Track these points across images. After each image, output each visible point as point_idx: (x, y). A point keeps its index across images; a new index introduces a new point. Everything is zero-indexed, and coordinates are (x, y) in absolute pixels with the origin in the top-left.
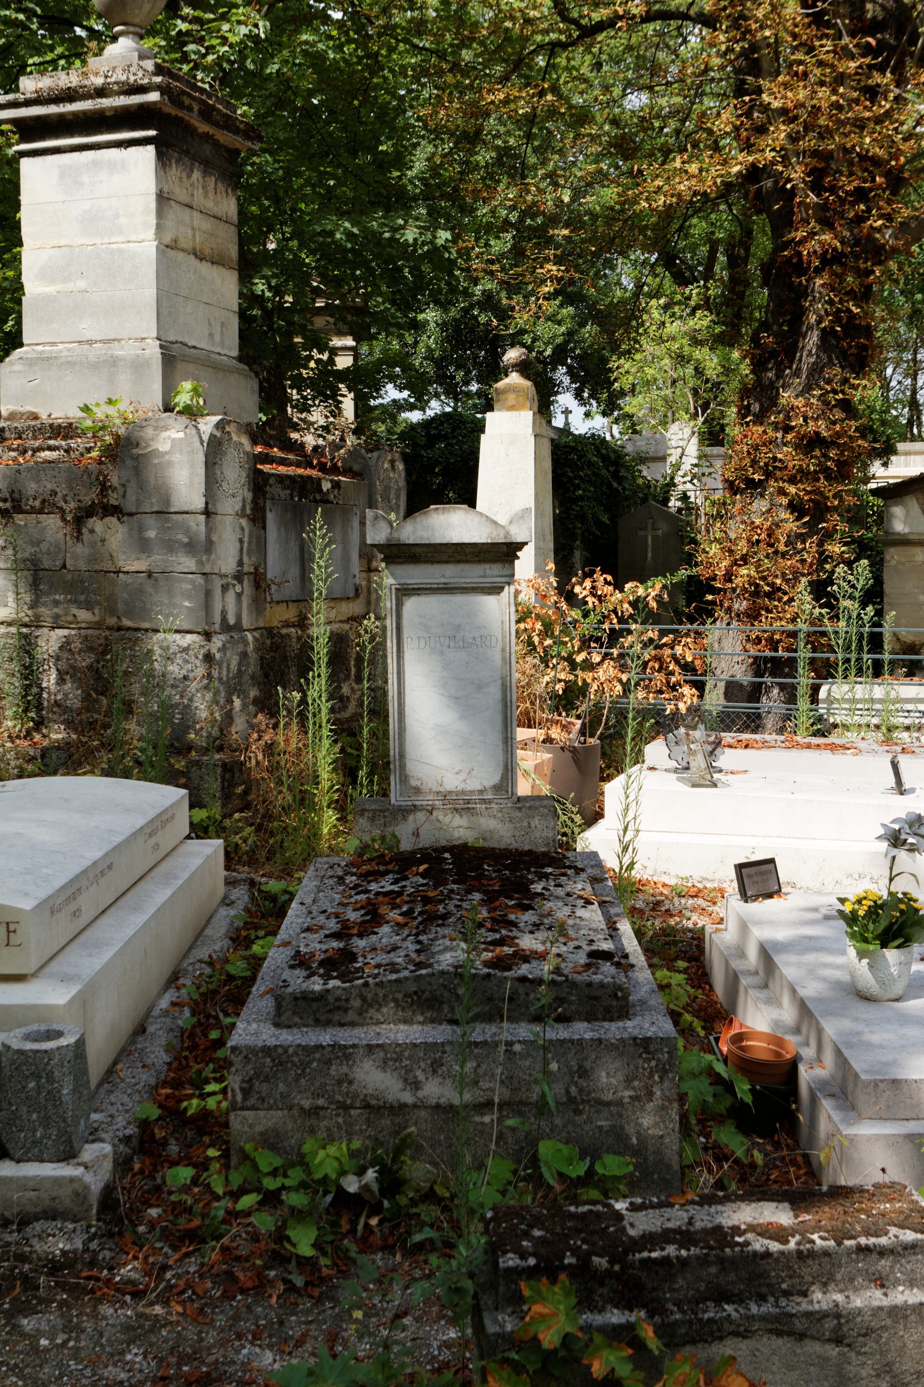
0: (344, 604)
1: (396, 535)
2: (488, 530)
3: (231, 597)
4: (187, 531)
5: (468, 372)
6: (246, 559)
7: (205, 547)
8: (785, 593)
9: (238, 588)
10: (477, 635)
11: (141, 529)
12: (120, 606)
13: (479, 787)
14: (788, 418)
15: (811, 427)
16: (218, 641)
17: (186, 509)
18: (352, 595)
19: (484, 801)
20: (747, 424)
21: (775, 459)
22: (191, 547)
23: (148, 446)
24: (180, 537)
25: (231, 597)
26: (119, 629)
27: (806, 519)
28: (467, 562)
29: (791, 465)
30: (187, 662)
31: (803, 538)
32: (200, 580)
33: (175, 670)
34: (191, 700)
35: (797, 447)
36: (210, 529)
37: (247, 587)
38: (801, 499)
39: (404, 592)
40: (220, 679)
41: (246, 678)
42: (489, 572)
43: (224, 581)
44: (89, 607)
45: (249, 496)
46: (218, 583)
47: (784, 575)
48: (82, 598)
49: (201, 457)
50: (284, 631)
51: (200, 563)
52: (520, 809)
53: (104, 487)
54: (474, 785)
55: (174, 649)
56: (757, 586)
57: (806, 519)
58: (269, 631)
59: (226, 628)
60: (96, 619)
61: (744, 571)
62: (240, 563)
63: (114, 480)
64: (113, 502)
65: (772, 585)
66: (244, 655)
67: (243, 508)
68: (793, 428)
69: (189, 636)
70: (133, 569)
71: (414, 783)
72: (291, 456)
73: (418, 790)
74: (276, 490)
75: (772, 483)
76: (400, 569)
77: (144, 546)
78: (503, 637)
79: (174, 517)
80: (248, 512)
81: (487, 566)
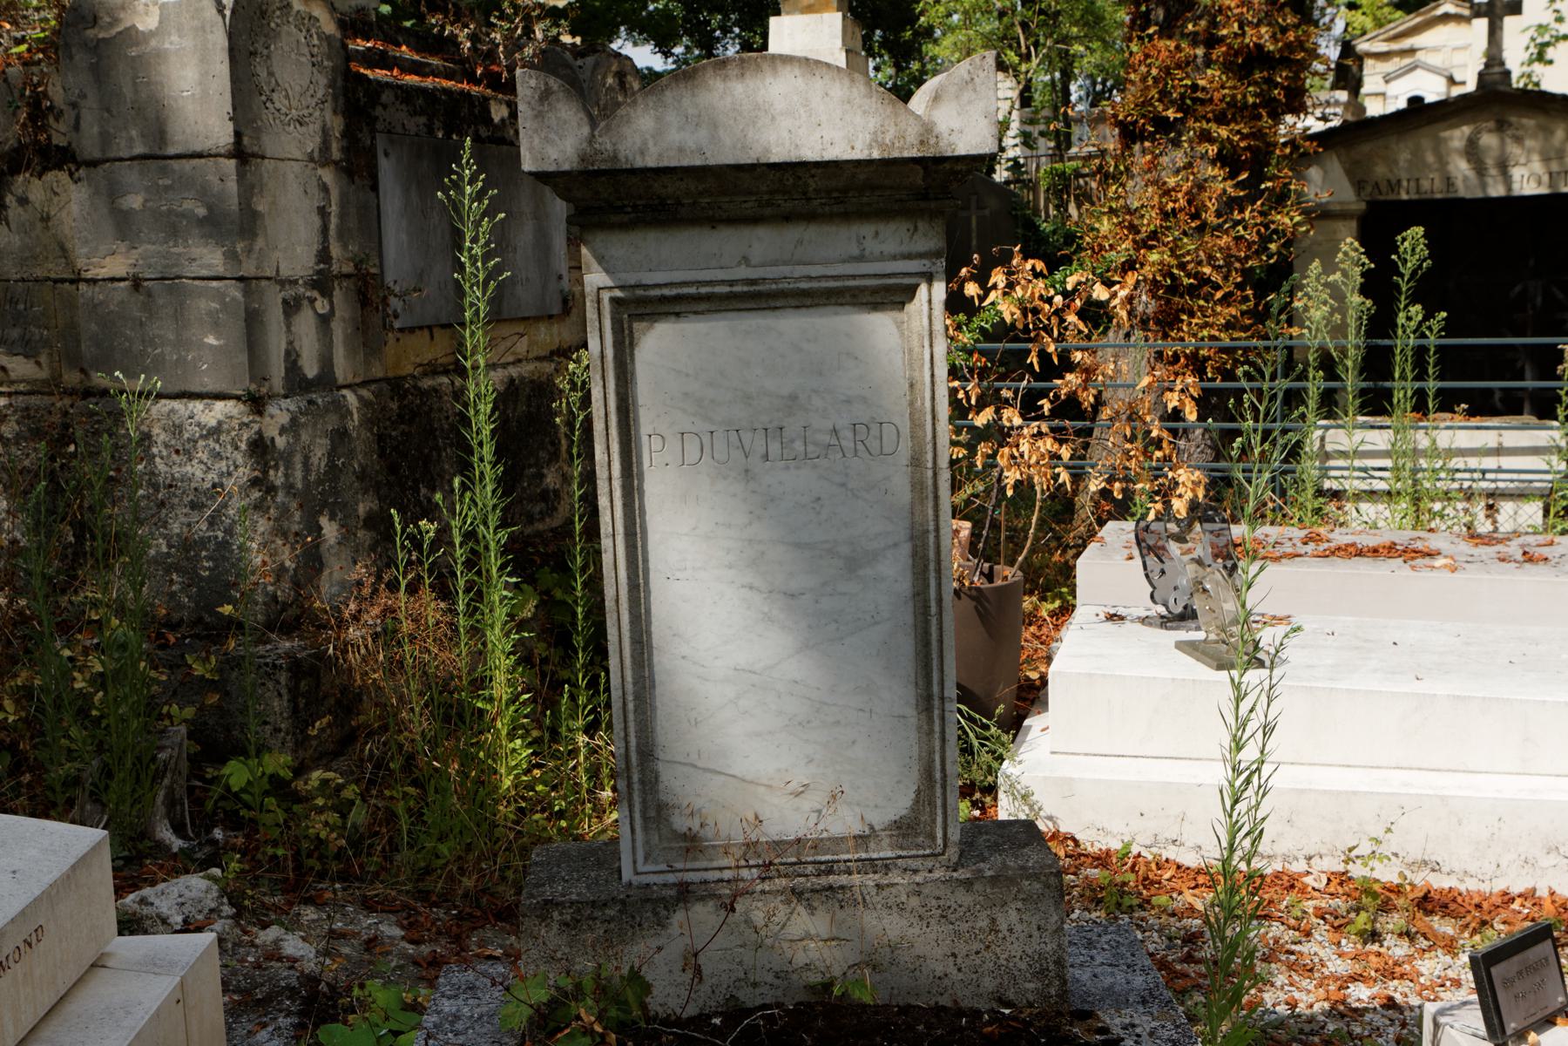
0: (543, 328)
1: (605, 143)
2: (872, 123)
3: (305, 323)
4: (203, 194)
5: (726, 17)
6: (335, 250)
7: (240, 225)
8: (1217, 287)
9: (322, 306)
10: (843, 422)
11: (113, 193)
12: (87, 348)
13: (857, 828)
14: (1213, 24)
15: (1250, 38)
16: (279, 414)
17: (198, 148)
18: (556, 309)
19: (871, 865)
20: (1151, 37)
21: (1195, 87)
22: (214, 225)
23: (116, 21)
24: (188, 205)
25: (305, 323)
26: (88, 393)
27: (1244, 176)
28: (811, 217)
29: (1217, 96)
30: (217, 456)
31: (1240, 204)
32: (235, 292)
33: (195, 471)
34: (229, 531)
35: (1227, 67)
36: (248, 189)
37: (342, 302)
38: (1235, 147)
39: (639, 307)
40: (289, 487)
41: (347, 480)
42: (872, 246)
43: (290, 292)
44: (28, 349)
45: (337, 124)
46: (273, 300)
47: (1211, 258)
48: (15, 333)
49: (219, 39)
50: (426, 383)
51: (231, 256)
52: (967, 884)
53: (39, 111)
54: (844, 822)
55: (191, 431)
56: (1172, 276)
57: (1244, 176)
58: (395, 385)
59: (297, 383)
60: (44, 374)
61: (1154, 257)
62: (324, 256)
63: (56, 93)
64: (59, 140)
65: (1197, 275)
66: (340, 437)
67: (325, 146)
68: (1221, 40)
69: (219, 405)
70: (103, 273)
71: (680, 823)
72: (435, 61)
73: (691, 843)
74: (397, 116)
75: (1191, 123)
76: (621, 245)
77: (124, 226)
78: (916, 425)
79: (175, 164)
80: (336, 154)
81: (867, 229)
